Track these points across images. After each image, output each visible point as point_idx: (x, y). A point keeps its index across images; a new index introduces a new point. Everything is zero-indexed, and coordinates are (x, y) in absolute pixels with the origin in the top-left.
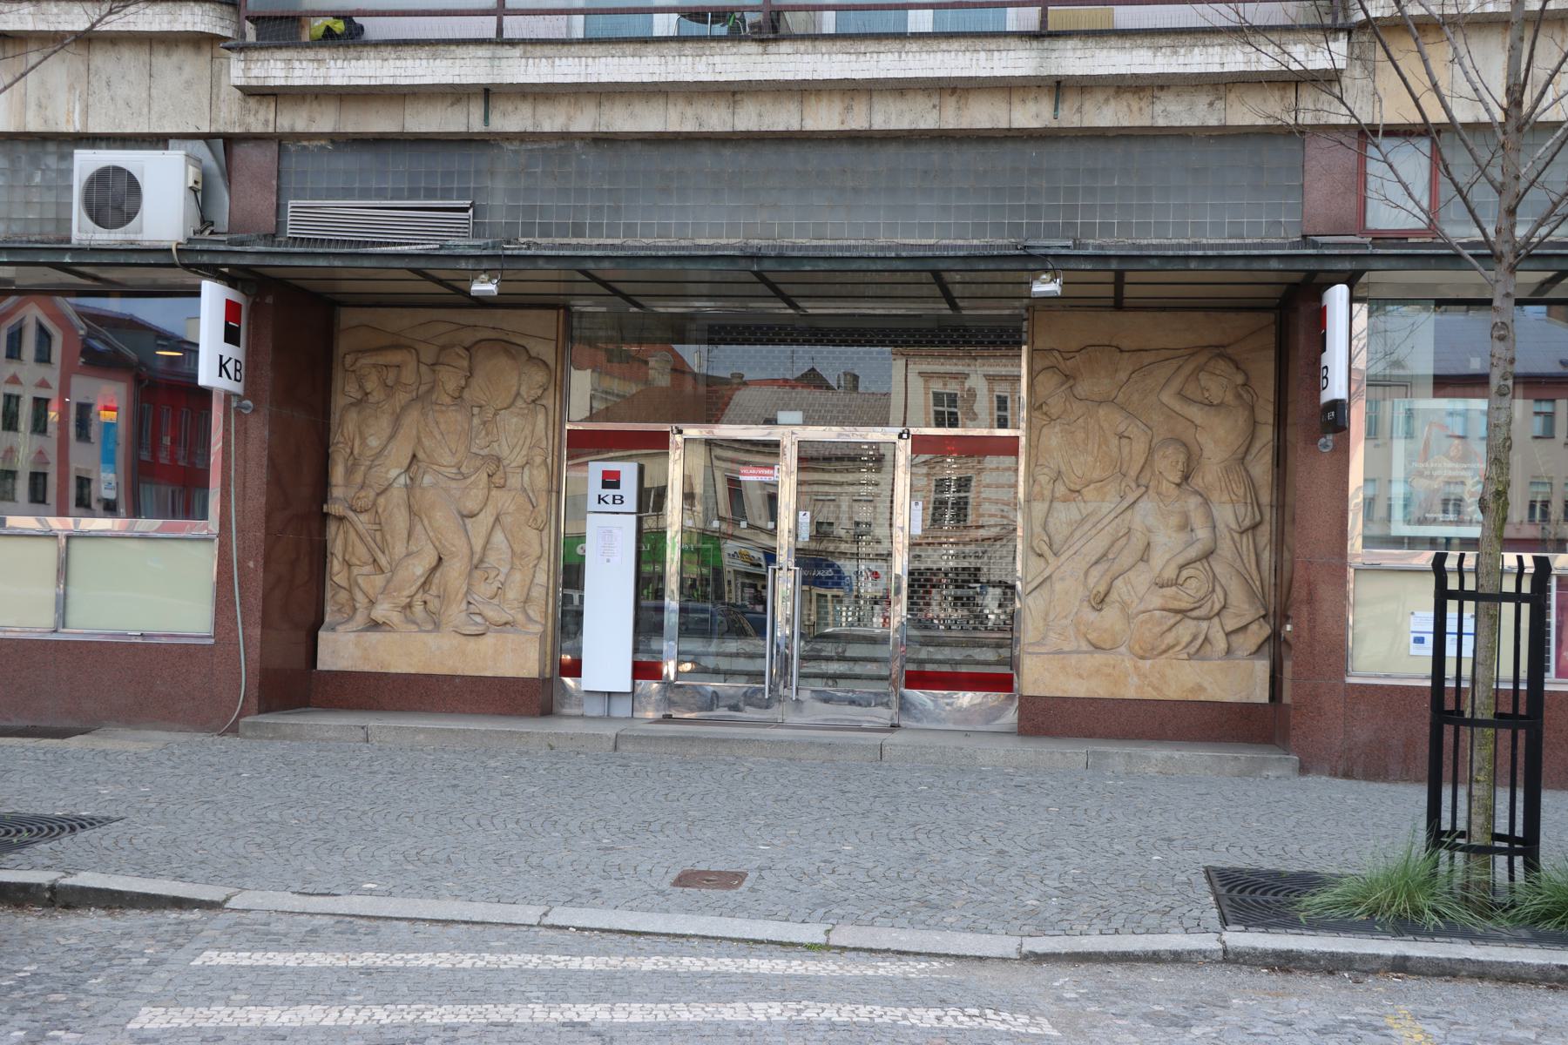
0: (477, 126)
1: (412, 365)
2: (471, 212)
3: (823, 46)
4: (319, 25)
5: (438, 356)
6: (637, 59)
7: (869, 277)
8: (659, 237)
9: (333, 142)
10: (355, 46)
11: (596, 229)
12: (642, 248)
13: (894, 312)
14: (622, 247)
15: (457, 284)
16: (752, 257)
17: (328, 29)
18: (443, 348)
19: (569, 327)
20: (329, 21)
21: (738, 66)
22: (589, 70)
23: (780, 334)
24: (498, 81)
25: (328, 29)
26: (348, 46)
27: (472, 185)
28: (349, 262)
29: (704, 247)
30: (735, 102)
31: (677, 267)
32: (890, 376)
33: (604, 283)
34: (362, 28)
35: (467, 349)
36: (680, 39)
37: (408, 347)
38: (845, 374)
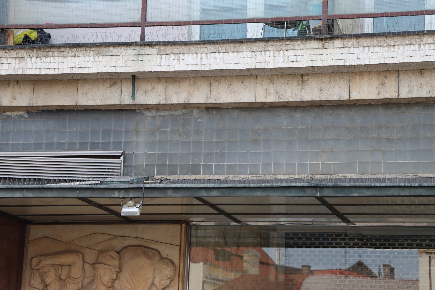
0: (127, 100)
1: (80, 264)
2: (122, 158)
3: (364, 42)
4: (20, 34)
5: (98, 259)
6: (236, 54)
7: (399, 201)
8: (251, 174)
9: (28, 112)
10: (44, 48)
11: (208, 169)
12: (239, 182)
13: (419, 225)
14: (225, 181)
15: (112, 208)
16: (315, 187)
17: (26, 37)
18: (101, 252)
19: (189, 236)
20: (27, 32)
21: (305, 57)
22: (203, 62)
23: (336, 239)
24: (141, 70)
25: (26, 37)
26: (40, 48)
27: (123, 140)
28: (37, 194)
29: (282, 180)
30: (303, 81)
31: (264, 194)
32: (418, 270)
33: (213, 206)
34: (49, 36)
35: (118, 253)
36: (265, 40)
37: (77, 252)
38: (384, 266)
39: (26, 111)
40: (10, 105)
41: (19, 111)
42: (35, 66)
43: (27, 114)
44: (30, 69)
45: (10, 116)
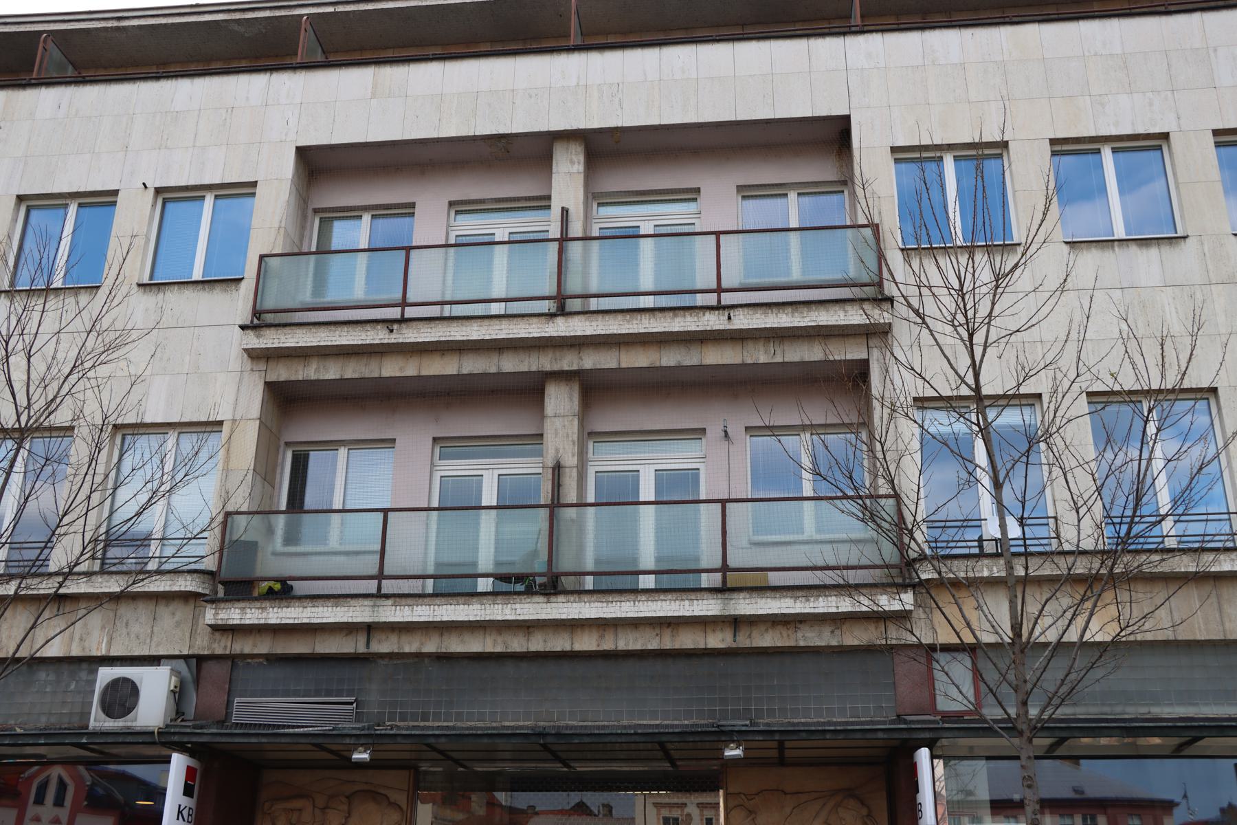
42: (276, 615)
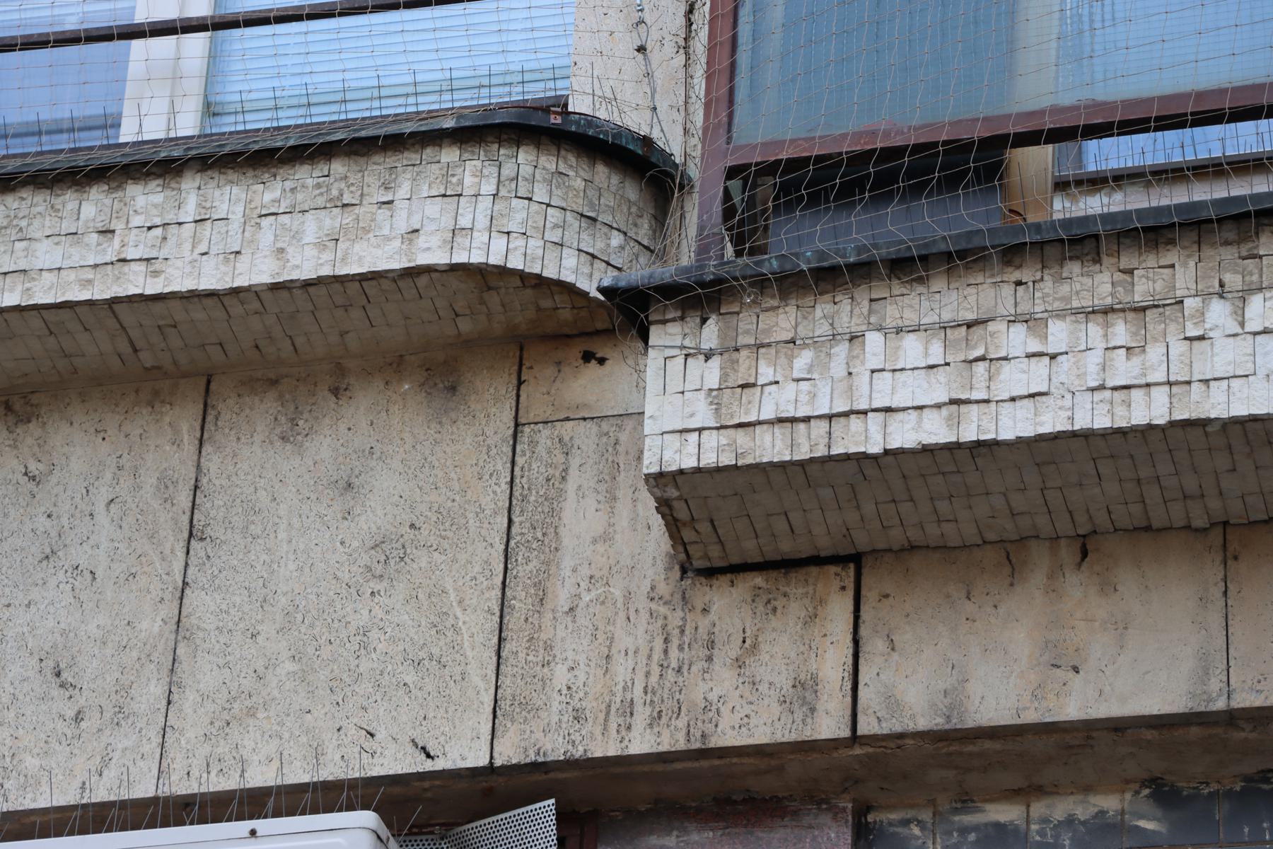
39: (1144, 784)
40: (1031, 717)
41: (1088, 789)
43: (1159, 813)
44: (1235, 383)
45: (1016, 830)
